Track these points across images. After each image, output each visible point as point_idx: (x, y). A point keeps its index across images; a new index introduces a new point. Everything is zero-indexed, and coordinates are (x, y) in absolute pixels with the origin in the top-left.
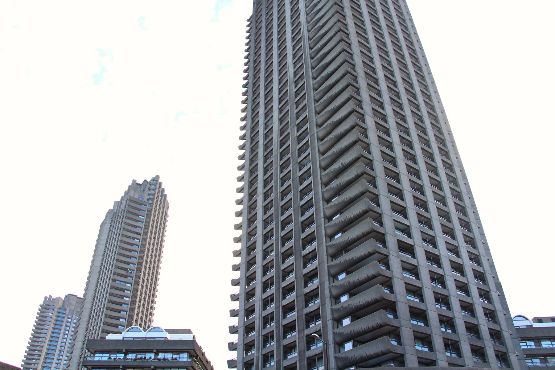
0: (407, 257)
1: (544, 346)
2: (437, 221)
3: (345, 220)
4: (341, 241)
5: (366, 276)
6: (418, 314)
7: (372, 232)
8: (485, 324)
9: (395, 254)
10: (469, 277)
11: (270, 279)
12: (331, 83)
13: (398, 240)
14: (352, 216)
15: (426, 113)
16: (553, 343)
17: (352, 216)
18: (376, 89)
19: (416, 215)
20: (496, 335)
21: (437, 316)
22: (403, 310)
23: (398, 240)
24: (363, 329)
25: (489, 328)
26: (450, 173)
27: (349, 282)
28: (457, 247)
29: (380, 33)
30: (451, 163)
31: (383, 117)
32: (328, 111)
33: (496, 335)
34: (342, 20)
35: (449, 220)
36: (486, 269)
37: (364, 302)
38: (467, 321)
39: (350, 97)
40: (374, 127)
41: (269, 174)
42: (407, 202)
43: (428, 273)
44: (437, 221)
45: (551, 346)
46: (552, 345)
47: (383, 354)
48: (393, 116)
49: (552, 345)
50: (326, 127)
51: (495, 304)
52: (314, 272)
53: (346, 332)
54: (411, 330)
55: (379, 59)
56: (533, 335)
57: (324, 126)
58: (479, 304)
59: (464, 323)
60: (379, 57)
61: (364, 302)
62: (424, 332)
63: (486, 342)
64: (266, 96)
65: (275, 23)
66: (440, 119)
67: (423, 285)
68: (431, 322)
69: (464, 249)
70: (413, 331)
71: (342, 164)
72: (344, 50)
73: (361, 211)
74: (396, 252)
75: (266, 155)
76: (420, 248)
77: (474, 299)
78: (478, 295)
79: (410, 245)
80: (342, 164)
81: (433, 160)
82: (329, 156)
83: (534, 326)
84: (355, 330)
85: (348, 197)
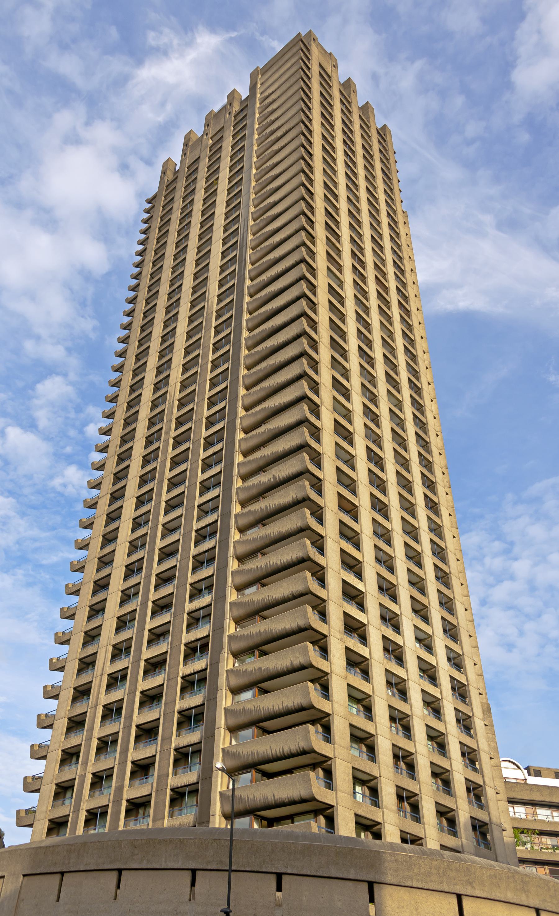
0: (355, 644)
1: (540, 818)
2: (405, 592)
3: (266, 566)
4: (255, 599)
5: (289, 664)
6: (363, 740)
7: (307, 594)
8: (461, 770)
9: (337, 635)
10: (443, 688)
11: (125, 641)
12: (276, 343)
13: (344, 612)
14: (279, 563)
15: (412, 416)
16: (555, 814)
17: (279, 563)
18: (344, 367)
19: (375, 577)
20: (475, 792)
21: (390, 747)
22: (340, 730)
23: (344, 612)
24: (274, 752)
25: (466, 779)
26: (433, 516)
27: (260, 669)
28: (430, 636)
29: (362, 275)
30: (437, 501)
31: (346, 412)
32: (264, 388)
33: (475, 792)
34: (308, 243)
35: (423, 591)
36: (470, 680)
37: (281, 707)
38: (435, 762)
39: (302, 373)
40: (332, 427)
41: (149, 468)
42: (365, 553)
43: (384, 673)
44: (405, 592)
45: (551, 819)
46: (553, 816)
47: (303, 801)
48: (362, 414)
49: (553, 816)
50: (256, 412)
51: (479, 739)
52: (203, 641)
53: (245, 752)
54: (350, 766)
55: (354, 319)
56: (526, 796)
57: (253, 411)
58: (454, 738)
59: (429, 764)
60: (354, 315)
61: (281, 707)
62: (368, 771)
63: (459, 801)
64: (164, 339)
65: (197, 218)
66: (430, 428)
67: (330, 633)
68: (381, 756)
69: (440, 642)
70: (353, 768)
71: (274, 477)
72: (304, 295)
73: (294, 557)
74: (340, 632)
75: (149, 436)
76: (376, 632)
77: (448, 726)
78: (455, 720)
79: (362, 623)
80: (274, 477)
81: (410, 491)
82: (254, 460)
83: (529, 782)
84: (260, 752)
85: (276, 531)
